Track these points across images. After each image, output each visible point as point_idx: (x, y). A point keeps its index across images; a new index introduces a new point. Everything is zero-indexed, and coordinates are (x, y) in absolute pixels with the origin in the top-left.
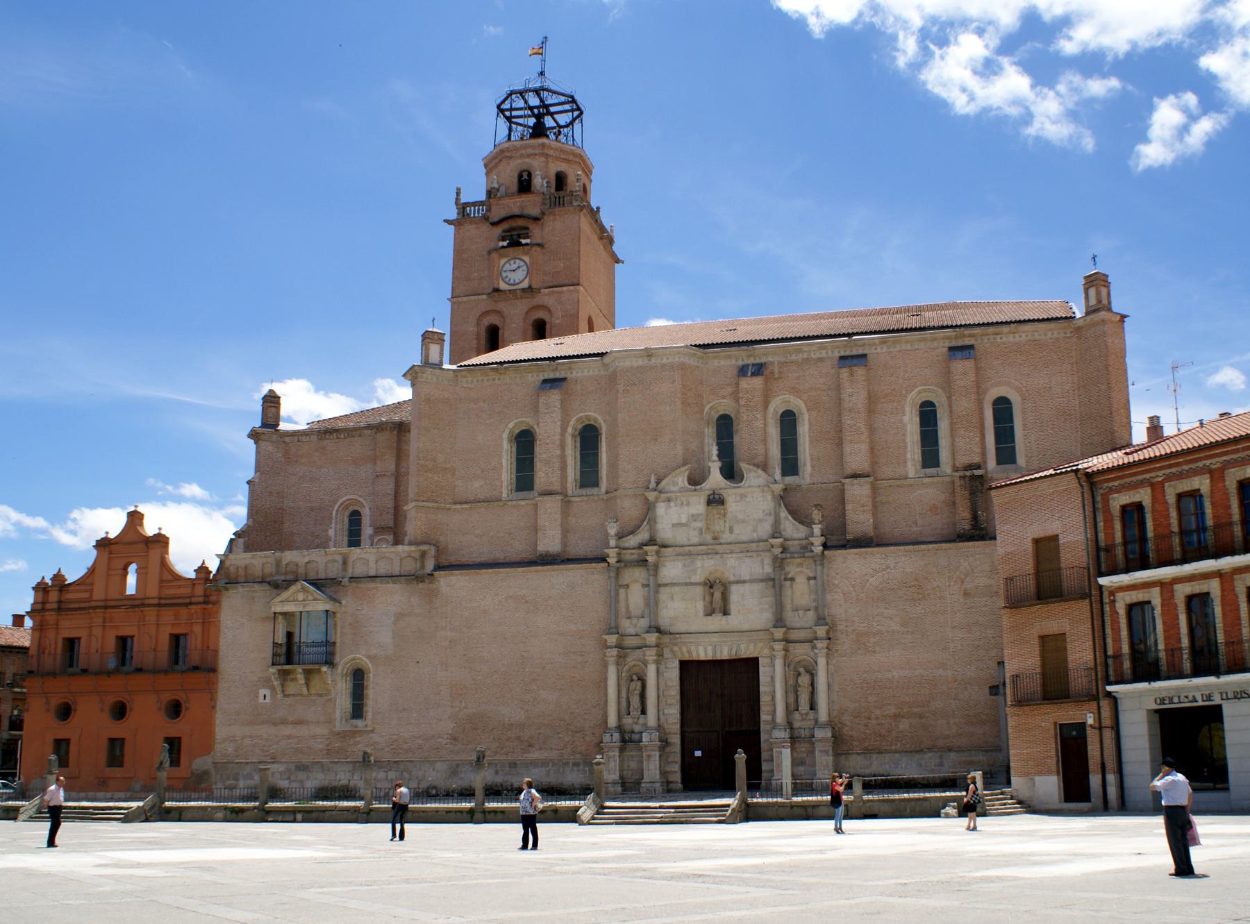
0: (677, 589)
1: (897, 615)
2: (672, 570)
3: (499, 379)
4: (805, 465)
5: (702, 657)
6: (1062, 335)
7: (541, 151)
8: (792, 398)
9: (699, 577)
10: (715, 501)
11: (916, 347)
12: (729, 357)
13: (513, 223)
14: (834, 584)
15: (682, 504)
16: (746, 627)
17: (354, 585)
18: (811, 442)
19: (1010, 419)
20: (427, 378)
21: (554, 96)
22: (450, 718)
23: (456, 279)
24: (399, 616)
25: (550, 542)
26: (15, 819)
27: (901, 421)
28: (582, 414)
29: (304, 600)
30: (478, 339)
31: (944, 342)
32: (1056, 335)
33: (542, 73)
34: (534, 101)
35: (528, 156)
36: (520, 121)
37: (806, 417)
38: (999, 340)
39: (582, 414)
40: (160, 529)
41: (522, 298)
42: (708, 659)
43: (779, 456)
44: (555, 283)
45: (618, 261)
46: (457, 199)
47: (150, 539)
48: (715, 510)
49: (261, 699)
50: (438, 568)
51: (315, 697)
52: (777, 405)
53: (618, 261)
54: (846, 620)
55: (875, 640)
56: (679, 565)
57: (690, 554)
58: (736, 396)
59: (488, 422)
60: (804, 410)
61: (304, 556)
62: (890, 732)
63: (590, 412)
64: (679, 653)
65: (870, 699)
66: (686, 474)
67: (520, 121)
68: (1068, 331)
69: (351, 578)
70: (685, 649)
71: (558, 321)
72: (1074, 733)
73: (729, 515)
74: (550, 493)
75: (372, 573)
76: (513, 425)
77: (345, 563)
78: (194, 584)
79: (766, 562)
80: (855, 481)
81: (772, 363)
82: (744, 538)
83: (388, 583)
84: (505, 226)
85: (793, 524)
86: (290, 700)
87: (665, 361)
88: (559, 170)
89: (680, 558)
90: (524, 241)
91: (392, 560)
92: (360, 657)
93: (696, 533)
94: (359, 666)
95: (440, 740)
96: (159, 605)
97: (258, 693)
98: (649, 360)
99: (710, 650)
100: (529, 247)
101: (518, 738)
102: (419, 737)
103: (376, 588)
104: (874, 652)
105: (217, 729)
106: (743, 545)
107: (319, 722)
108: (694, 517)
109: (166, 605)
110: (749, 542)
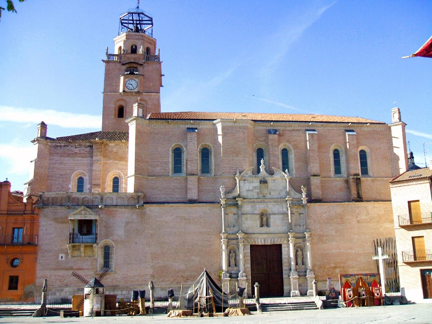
0: (249, 216)
1: (333, 229)
2: (247, 208)
3: (168, 126)
4: (292, 170)
5: (260, 244)
6: (384, 129)
7: (141, 38)
8: (288, 144)
9: (258, 211)
10: (264, 182)
11: (333, 128)
12: (263, 126)
13: (132, 65)
14: (310, 216)
15: (250, 182)
16: (276, 231)
17: (106, 209)
18: (295, 161)
19: (366, 158)
20: (139, 122)
21: (146, 17)
22: (151, 267)
23: (106, 85)
24: (127, 223)
25: (193, 195)
26: (228, 316)
27: (328, 156)
28: (204, 143)
29: (85, 214)
30: (115, 110)
31: (343, 128)
32: (382, 129)
33: (138, 7)
34: (136, 17)
35: (137, 39)
36: (126, 25)
37: (293, 151)
38: (362, 129)
39: (204, 143)
40: (7, 179)
41: (134, 96)
42: (262, 244)
43: (282, 166)
44: (149, 91)
45: (161, 86)
46: (107, 52)
47: (3, 184)
48: (263, 185)
49: (60, 258)
50: (145, 203)
51: (87, 258)
52: (281, 147)
53: (161, 86)
54: (315, 230)
55: (326, 238)
56: (250, 206)
57: (254, 202)
58: (266, 141)
59: (163, 143)
60: (292, 148)
61: (82, 195)
62: (332, 273)
63: (207, 142)
64: (250, 242)
65: (325, 261)
66: (252, 170)
67: (126, 25)
68: (386, 128)
69: (105, 205)
70: (253, 240)
71: (149, 107)
72: (427, 273)
73: (269, 187)
74: (193, 175)
75: (114, 204)
76: (173, 145)
77: (102, 199)
78: (26, 205)
79: (284, 207)
80: (315, 177)
81: (280, 130)
82: (275, 197)
83: (123, 208)
84: (128, 66)
85: (294, 192)
86: (75, 259)
87: (241, 125)
88: (148, 46)
89: (250, 203)
90: (135, 73)
91: (124, 198)
92: (109, 241)
93: (256, 194)
94: (108, 245)
95: (146, 277)
96: (7, 214)
97: (59, 255)
98: (234, 124)
99: (263, 241)
100: (138, 76)
101: (182, 276)
102: (137, 276)
103: (117, 211)
104: (326, 243)
105: (37, 272)
106: (275, 200)
107: (89, 269)
108: (255, 188)
109: (11, 214)
110: (277, 199)
